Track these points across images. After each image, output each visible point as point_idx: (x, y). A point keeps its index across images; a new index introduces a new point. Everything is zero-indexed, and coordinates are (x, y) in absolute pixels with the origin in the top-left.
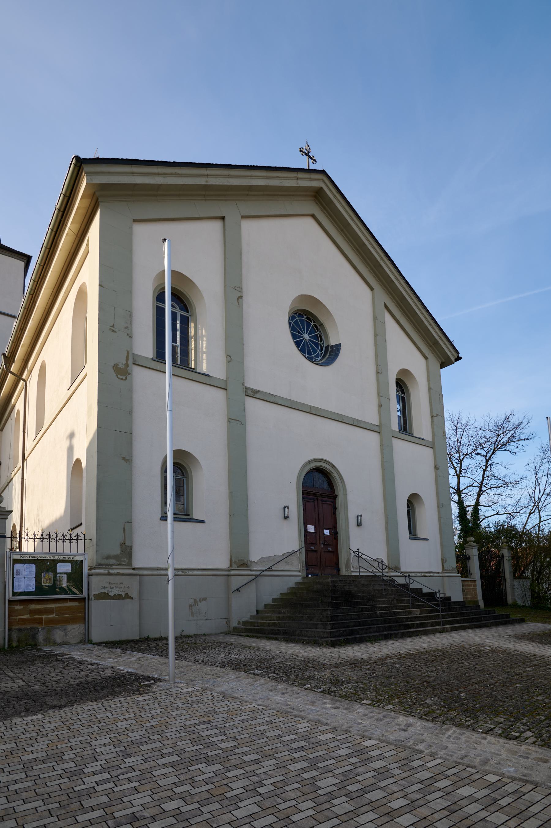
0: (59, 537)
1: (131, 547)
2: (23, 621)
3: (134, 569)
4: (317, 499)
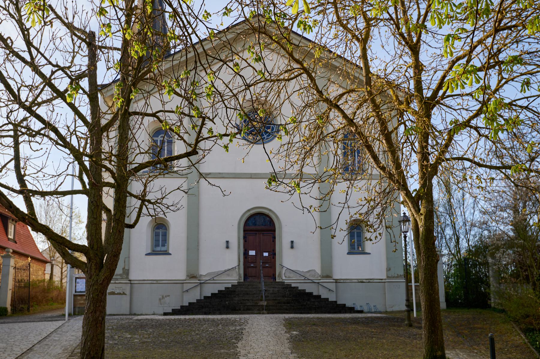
1: (128, 270)
2: (81, 304)
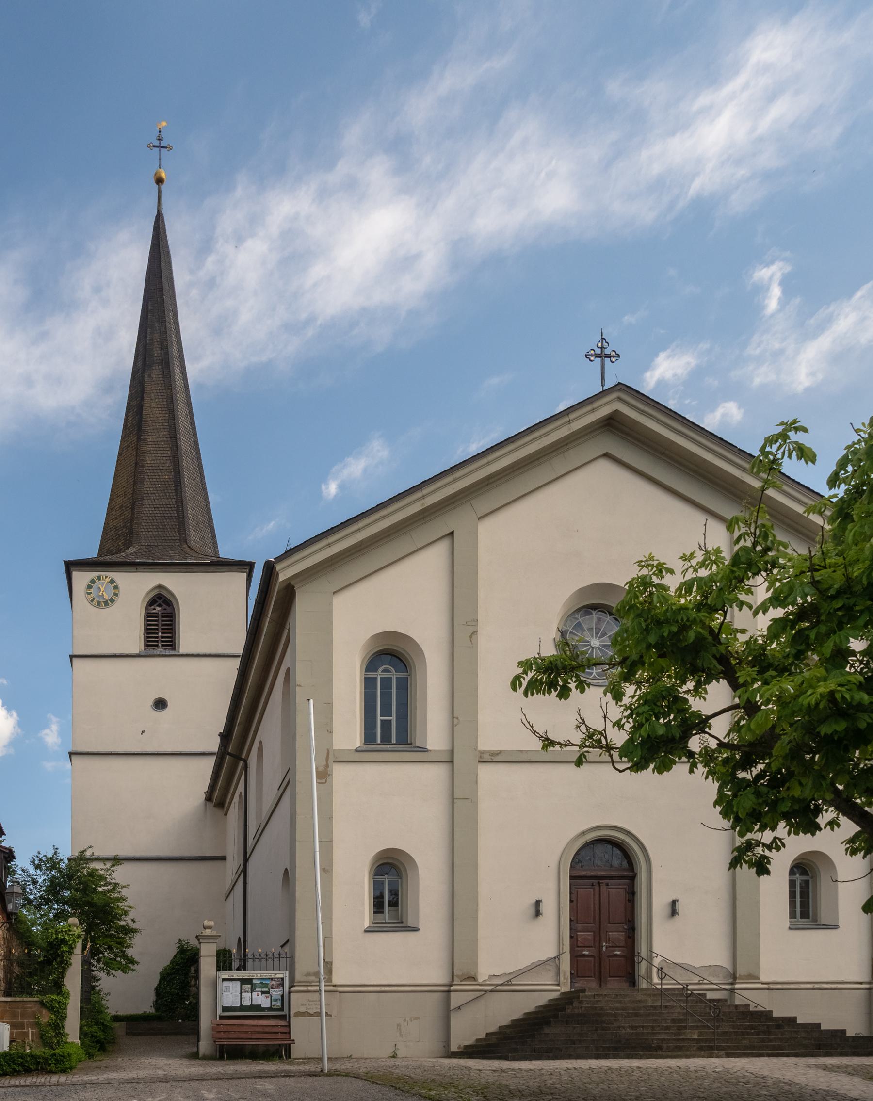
0: (262, 956)
1: (331, 963)
3: (334, 986)
4: (599, 883)
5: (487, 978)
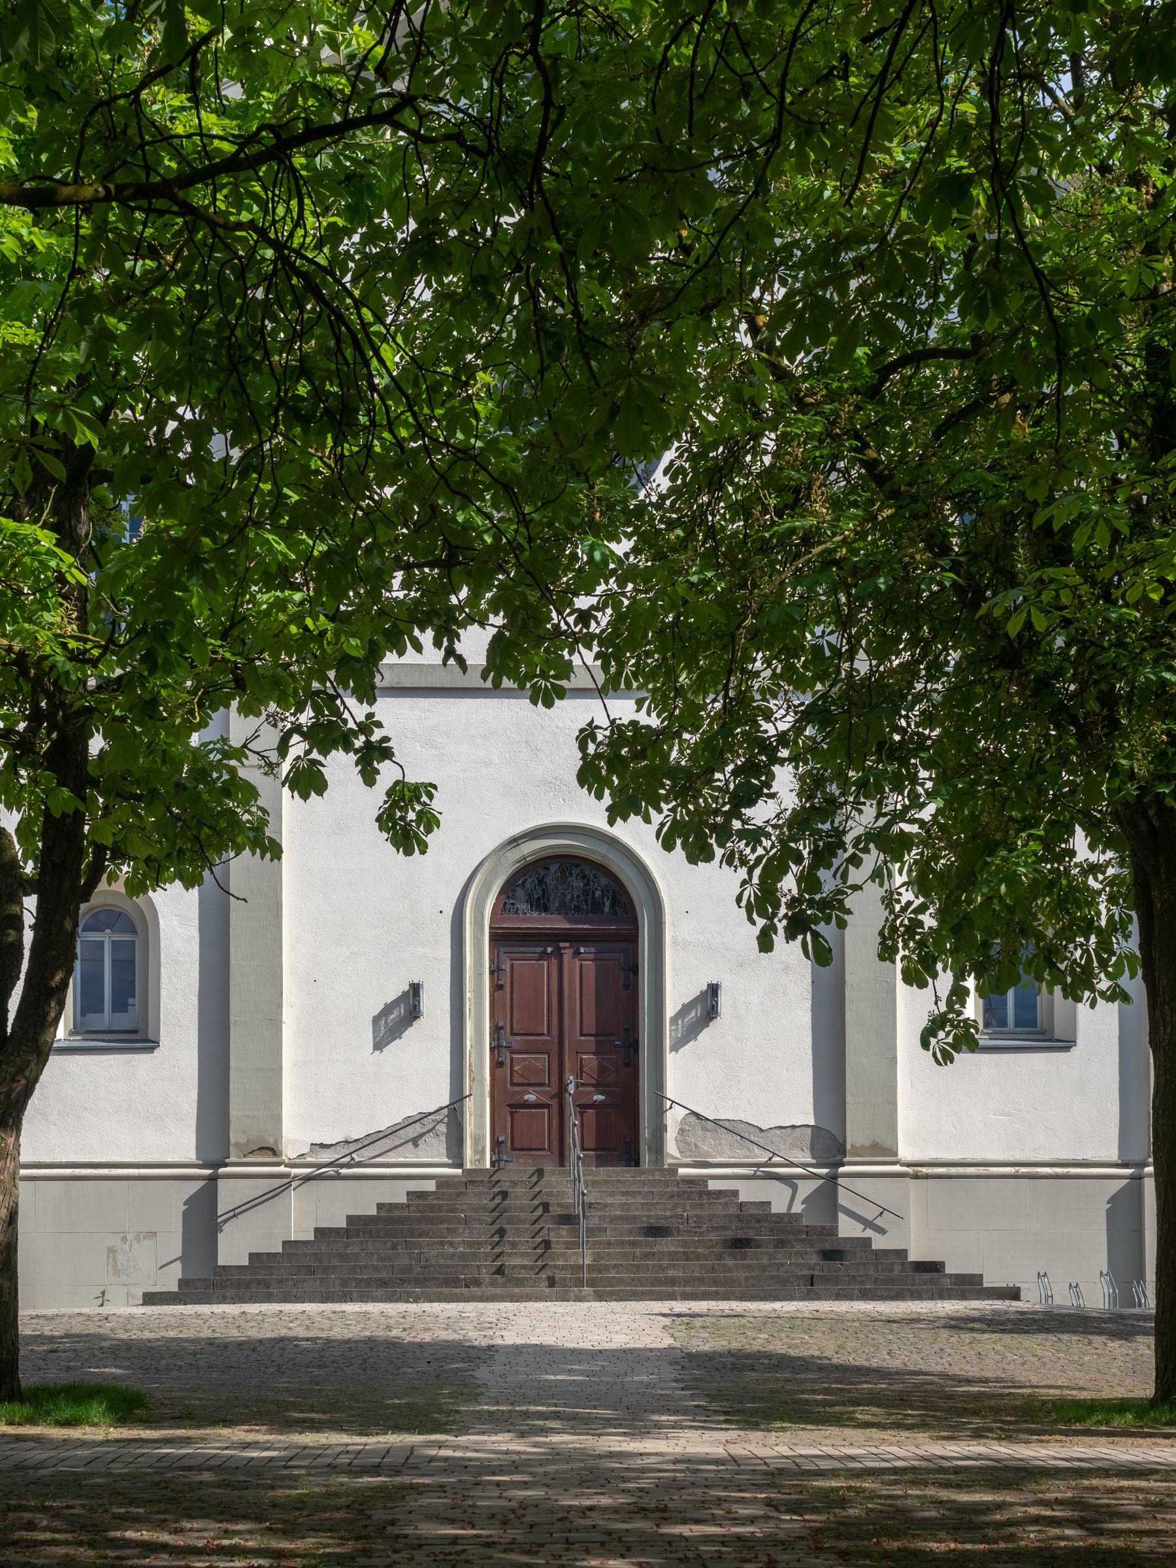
5: (306, 1150)
